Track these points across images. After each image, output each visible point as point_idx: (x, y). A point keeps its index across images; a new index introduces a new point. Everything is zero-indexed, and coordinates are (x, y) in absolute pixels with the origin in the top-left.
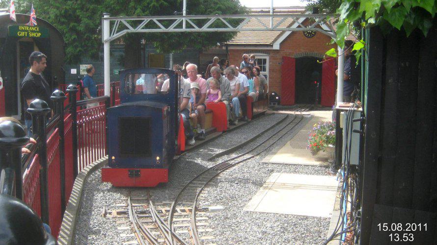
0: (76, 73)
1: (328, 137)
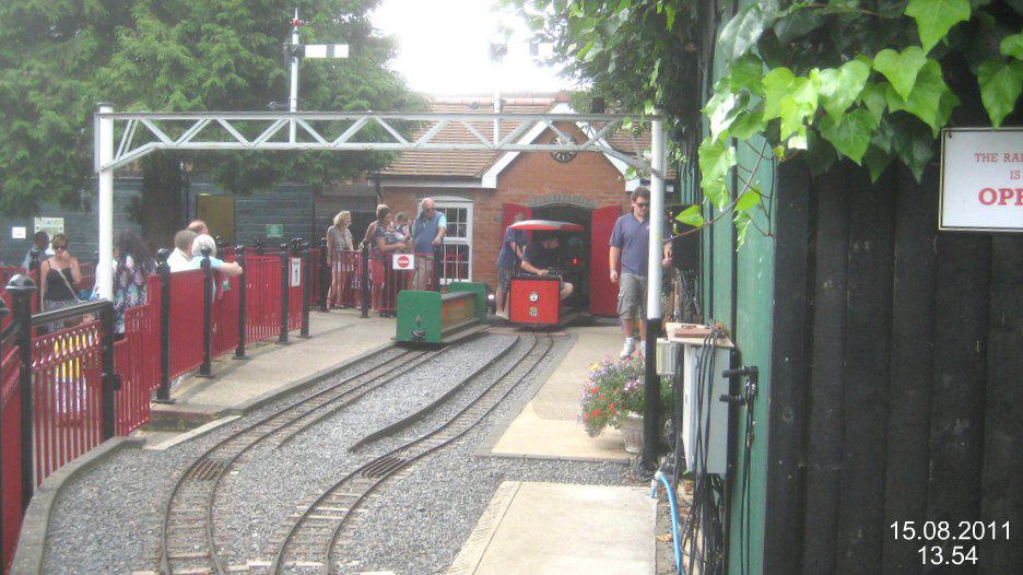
1: (625, 396)
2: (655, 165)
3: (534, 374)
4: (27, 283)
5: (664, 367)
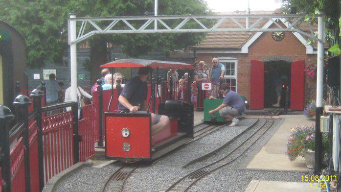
0: (39, 78)
1: (306, 142)
2: (319, 37)
3: (265, 135)
4: (40, 93)
5: (324, 129)
